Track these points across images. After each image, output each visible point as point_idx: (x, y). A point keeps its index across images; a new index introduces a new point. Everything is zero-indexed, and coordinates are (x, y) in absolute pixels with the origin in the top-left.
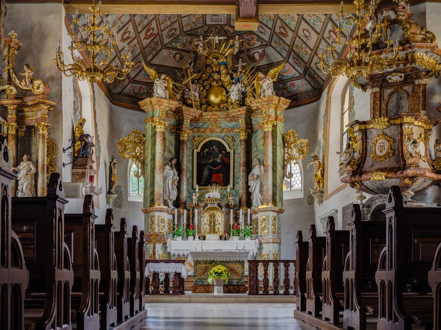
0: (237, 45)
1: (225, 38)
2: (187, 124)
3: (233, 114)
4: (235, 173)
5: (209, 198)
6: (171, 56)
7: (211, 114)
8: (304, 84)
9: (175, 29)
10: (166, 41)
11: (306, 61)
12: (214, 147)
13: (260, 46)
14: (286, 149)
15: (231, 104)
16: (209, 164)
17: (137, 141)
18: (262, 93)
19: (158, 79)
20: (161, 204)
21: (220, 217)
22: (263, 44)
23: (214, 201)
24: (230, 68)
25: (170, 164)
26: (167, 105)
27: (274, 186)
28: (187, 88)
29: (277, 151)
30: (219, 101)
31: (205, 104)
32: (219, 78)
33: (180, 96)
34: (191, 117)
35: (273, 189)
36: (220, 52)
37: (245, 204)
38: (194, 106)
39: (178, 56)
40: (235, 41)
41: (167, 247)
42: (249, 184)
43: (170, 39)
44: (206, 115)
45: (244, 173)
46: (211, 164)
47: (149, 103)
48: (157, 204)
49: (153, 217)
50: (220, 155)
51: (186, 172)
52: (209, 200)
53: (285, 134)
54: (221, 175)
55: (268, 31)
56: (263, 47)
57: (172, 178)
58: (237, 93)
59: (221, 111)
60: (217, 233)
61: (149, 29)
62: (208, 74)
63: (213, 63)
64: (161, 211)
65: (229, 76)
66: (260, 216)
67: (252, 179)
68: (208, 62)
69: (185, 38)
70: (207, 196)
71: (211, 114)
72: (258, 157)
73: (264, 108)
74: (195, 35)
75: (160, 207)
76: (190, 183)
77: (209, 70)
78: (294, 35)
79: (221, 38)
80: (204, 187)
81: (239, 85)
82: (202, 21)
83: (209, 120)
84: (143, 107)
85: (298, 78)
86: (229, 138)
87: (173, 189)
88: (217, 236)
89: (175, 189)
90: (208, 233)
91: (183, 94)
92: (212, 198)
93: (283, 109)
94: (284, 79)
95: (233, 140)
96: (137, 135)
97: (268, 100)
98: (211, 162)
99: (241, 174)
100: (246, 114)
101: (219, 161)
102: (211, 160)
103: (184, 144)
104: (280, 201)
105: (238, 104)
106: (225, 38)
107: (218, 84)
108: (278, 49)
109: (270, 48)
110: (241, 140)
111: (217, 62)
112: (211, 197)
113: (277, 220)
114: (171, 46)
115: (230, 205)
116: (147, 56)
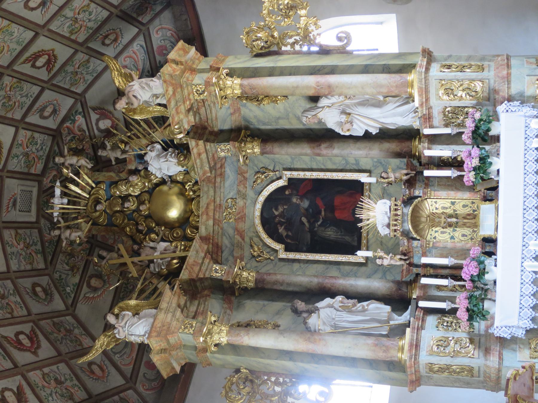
0: (73, 160)
1: (58, 184)
2: (222, 271)
3: (207, 168)
4: (334, 167)
5: (388, 226)
6: (91, 296)
7: (205, 217)
8: (160, 27)
9: (35, 285)
10: (58, 304)
11: (105, 14)
12: (276, 213)
13: (84, 116)
14: (284, 48)
15: (186, 176)
16: (312, 224)
17: (247, 388)
18: (158, 101)
19: (116, 331)
20: (401, 343)
21: (436, 202)
22: (81, 110)
23: (396, 215)
24: (117, 175)
25: (305, 315)
26: (170, 315)
27: (366, 69)
28: (148, 266)
29: (286, 67)
30: (178, 198)
31: (184, 230)
32: (135, 199)
33: (163, 283)
34: (207, 261)
35: (373, 72)
36: (85, 195)
37: (407, 144)
38: (184, 255)
39: (94, 282)
40: (66, 164)
41: (513, 337)
42: (361, 133)
43: (57, 296)
44: (206, 228)
45: (336, 145)
46: (312, 220)
47: (163, 355)
48: (400, 355)
49: (430, 367)
50: (294, 200)
51: (326, 277)
52: (396, 225)
53: (252, 52)
54: (338, 200)
55: (48, 95)
56: (86, 111)
57: (339, 313)
58: (162, 160)
59: (199, 196)
60: (474, 211)
61: (16, 342)
62: (126, 221)
63: (105, 211)
64: (417, 346)
65: (131, 179)
66: (439, 102)
67: (348, 126)
68: (104, 220)
69: (59, 266)
70: (384, 231)
71: (205, 217)
72: (300, 114)
73: (191, 97)
74: (56, 246)
75: (406, 347)
76: (351, 271)
77: (117, 220)
78: (46, 34)
79: (58, 192)
80: (363, 238)
81: (151, 156)
82: (28, 231)
83: (216, 222)
84: (173, 368)
85: (148, 39)
86: (259, 181)
87: (364, 310)
88: (486, 208)
89: (363, 307)
90: (474, 231)
91: (159, 276)
92: (389, 218)
93: (197, 57)
94: (150, 70)
95: (263, 171)
96: (234, 387)
97: (172, 85)
98: (309, 222)
99: (336, 151)
100: (207, 140)
101: (306, 204)
102: (304, 220)
103: (264, 280)
104: (403, 57)
105: (185, 158)
106: (58, 184)
107: (147, 202)
108: (90, 78)
109: (88, 96)
110: (263, 153)
111: (105, 202)
112: (386, 221)
113: (448, 63)
114: (73, 295)
115: (408, 176)
116: (80, 348)
